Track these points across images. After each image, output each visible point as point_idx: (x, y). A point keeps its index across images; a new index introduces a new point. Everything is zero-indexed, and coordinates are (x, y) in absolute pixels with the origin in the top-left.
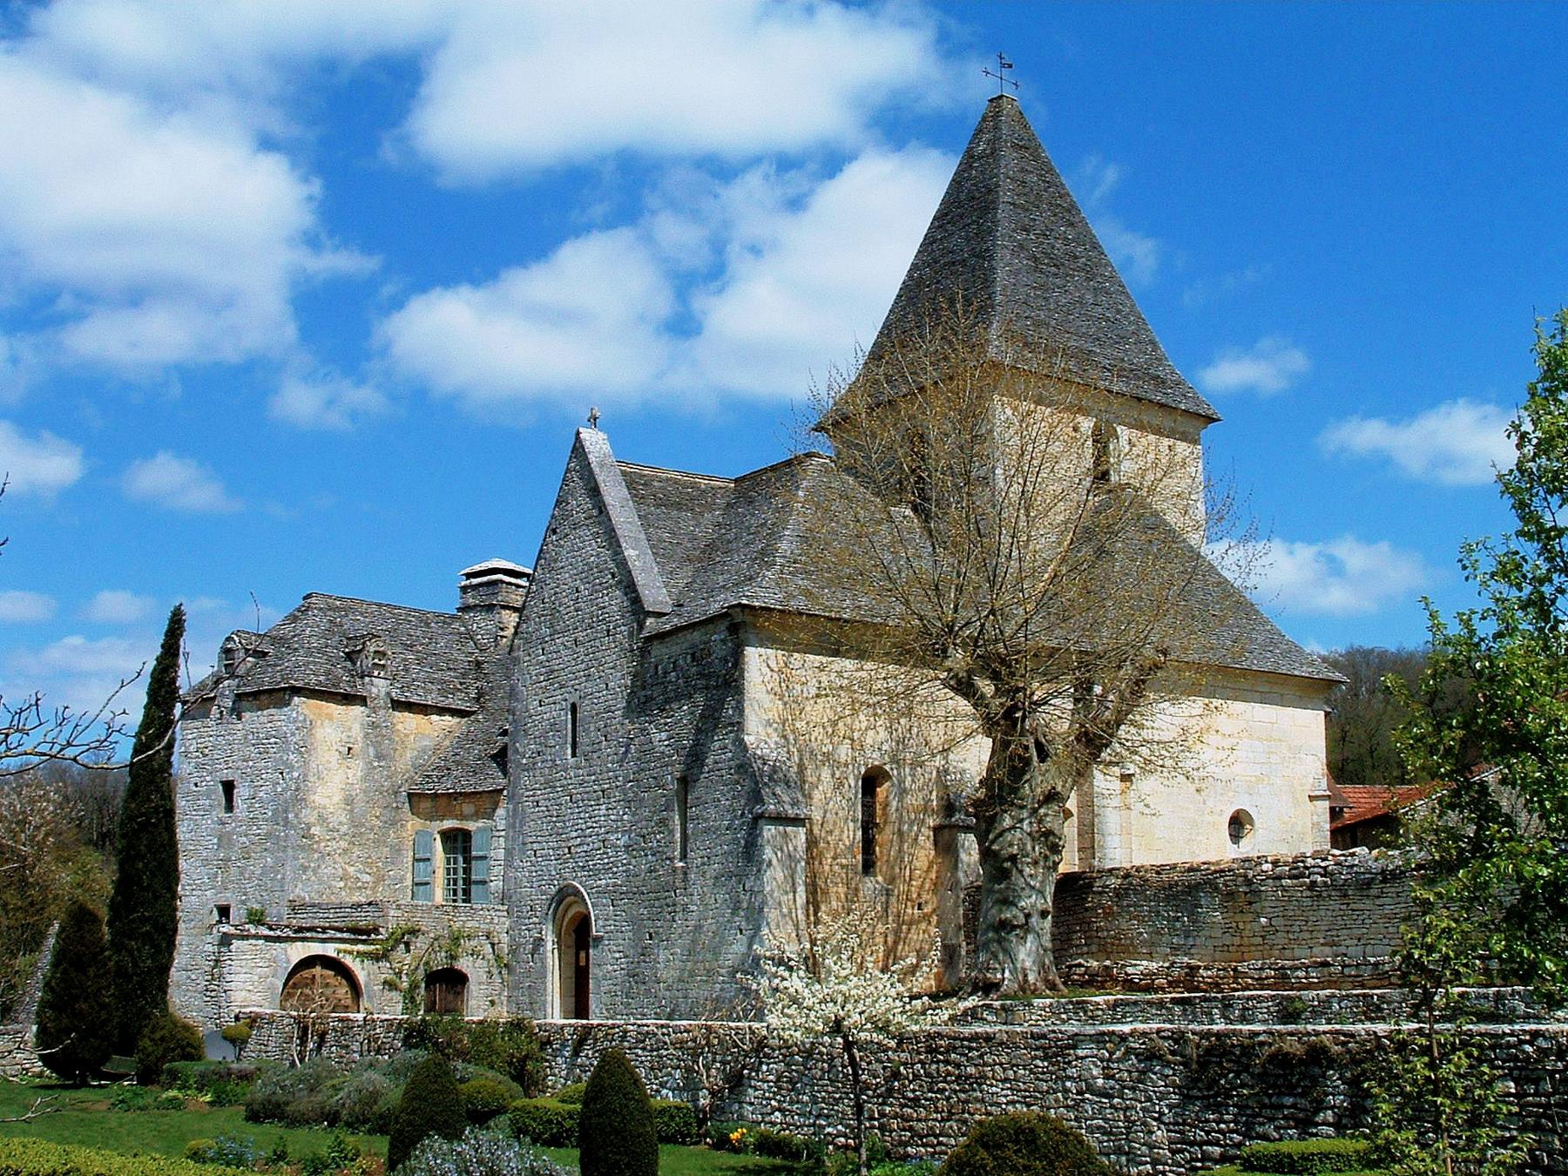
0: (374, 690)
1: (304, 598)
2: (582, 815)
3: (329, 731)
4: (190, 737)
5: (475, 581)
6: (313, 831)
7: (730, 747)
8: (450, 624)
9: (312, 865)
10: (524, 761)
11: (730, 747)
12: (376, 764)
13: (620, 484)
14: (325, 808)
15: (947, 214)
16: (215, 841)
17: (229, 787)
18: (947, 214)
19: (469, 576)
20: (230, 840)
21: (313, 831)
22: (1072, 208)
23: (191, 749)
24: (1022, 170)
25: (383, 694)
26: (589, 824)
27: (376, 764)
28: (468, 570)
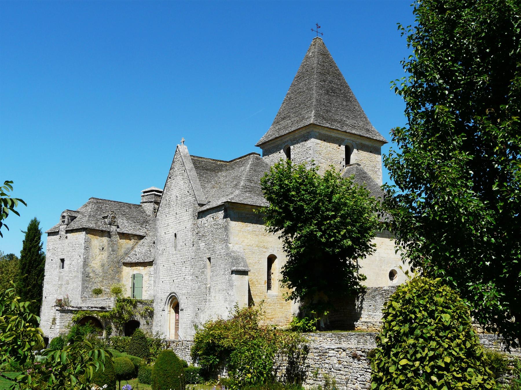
0: (112, 229)
1: (89, 199)
2: (177, 270)
3: (96, 242)
4: (50, 244)
5: (146, 194)
6: (90, 275)
7: (224, 248)
8: (138, 208)
9: (90, 286)
10: (160, 252)
11: (224, 248)
12: (112, 253)
13: (191, 163)
14: (94, 267)
15: (299, 76)
16: (58, 278)
17: (63, 260)
18: (299, 76)
19: (144, 192)
20: (62, 278)
21: (90, 275)
22: (340, 75)
23: (51, 248)
24: (323, 62)
25: (114, 230)
26: (180, 273)
27: (112, 253)
28: (144, 190)
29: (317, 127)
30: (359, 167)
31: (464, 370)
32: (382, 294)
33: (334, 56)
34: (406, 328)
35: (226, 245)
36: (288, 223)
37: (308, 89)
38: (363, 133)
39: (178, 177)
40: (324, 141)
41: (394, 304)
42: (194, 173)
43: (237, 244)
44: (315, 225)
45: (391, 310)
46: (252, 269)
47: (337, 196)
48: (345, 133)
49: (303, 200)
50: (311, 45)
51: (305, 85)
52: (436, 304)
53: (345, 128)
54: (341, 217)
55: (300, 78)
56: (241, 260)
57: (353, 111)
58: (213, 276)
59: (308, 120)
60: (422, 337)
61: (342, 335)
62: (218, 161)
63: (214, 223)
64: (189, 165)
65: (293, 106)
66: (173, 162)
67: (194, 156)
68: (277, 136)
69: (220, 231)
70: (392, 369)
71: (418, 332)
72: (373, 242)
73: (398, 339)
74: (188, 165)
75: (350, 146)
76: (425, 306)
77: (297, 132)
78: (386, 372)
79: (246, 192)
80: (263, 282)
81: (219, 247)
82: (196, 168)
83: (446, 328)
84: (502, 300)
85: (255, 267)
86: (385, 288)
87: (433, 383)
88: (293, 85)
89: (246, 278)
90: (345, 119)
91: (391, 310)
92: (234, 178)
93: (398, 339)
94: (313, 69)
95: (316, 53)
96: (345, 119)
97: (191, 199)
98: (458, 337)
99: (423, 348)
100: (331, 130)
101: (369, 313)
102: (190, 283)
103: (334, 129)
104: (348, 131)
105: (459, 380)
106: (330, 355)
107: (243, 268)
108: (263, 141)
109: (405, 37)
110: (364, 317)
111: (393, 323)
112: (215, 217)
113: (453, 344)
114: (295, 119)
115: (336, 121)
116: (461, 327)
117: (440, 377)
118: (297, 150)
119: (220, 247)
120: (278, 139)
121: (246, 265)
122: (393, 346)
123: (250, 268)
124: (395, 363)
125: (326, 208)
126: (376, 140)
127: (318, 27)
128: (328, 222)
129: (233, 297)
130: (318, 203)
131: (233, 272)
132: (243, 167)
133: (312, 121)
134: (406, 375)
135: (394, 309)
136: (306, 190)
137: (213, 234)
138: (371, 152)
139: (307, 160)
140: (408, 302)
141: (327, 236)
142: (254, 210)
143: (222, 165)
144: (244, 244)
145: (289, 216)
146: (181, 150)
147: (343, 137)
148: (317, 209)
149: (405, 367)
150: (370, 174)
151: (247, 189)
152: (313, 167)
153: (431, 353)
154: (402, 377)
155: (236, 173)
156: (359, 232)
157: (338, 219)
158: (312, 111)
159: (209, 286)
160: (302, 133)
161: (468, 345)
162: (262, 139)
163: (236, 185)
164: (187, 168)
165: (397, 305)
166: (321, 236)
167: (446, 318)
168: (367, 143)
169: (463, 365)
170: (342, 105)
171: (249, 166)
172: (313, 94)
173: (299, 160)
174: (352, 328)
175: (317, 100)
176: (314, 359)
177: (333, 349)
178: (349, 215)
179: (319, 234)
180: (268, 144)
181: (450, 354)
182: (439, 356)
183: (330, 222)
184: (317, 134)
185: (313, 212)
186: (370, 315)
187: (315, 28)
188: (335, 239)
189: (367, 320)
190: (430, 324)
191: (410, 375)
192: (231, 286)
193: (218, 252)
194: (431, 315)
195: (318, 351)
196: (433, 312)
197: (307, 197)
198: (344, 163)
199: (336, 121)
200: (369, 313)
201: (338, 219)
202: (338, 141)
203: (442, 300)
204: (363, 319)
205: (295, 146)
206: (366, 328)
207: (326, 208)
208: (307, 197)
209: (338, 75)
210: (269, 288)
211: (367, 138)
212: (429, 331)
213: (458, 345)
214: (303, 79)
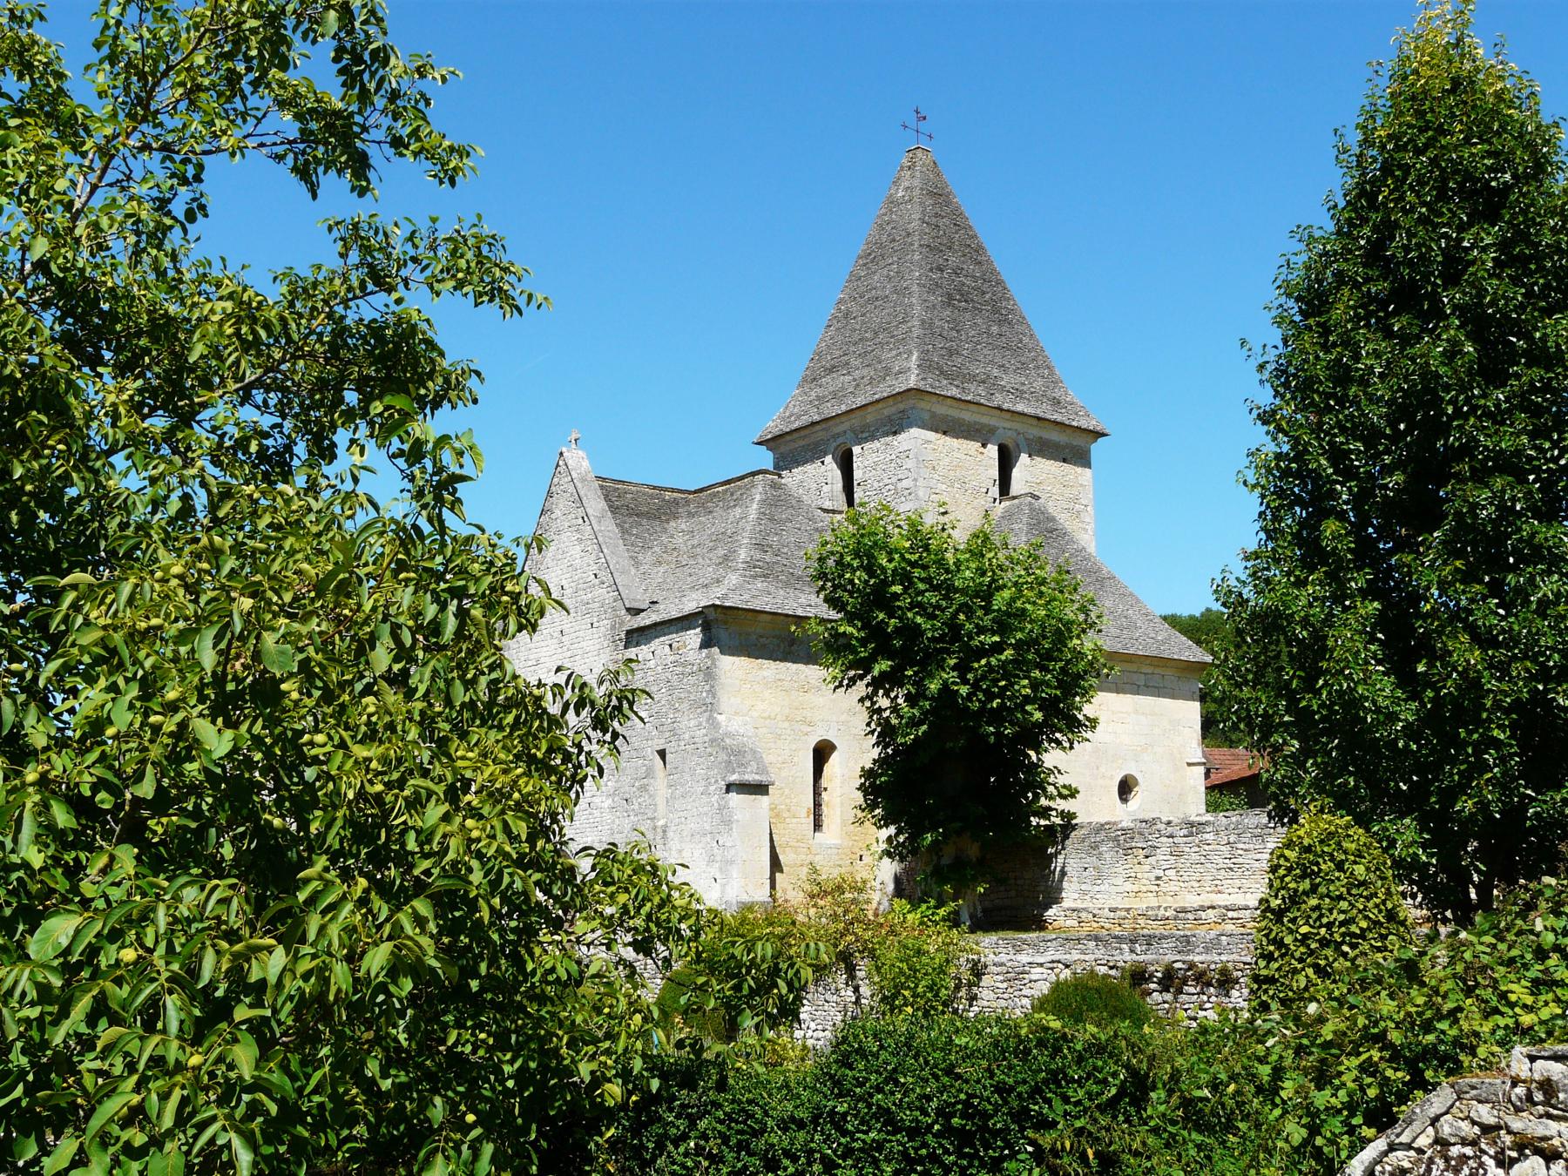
22: (980, 249)
29: (927, 398)
30: (1036, 504)
31: (1383, 937)
32: (1116, 839)
33: (963, 199)
34: (1305, 885)
35: (711, 717)
36: (883, 665)
37: (895, 292)
38: (1045, 411)
39: (564, 537)
40: (945, 433)
41: (1287, 853)
42: (608, 527)
43: (736, 713)
44: (954, 668)
45: (1282, 862)
46: (776, 776)
47: (1006, 594)
48: (998, 412)
49: (921, 608)
50: (902, 169)
51: (890, 279)
52: (1345, 852)
53: (998, 399)
54: (1015, 647)
55: (872, 257)
56: (749, 757)
57: (1017, 350)
58: (673, 797)
59: (902, 377)
60: (1328, 896)
61: (1024, 942)
62: (666, 489)
63: (672, 658)
64: (596, 505)
65: (856, 337)
66: (550, 494)
67: (604, 479)
68: (816, 418)
69: (692, 680)
70: (1288, 940)
71: (1322, 889)
72: (1088, 710)
73: (1295, 899)
74: (593, 503)
75: (1011, 445)
76: (1331, 855)
77: (870, 409)
78: (1279, 943)
79: (755, 577)
80: (803, 813)
81: (691, 724)
82: (614, 509)
83: (1363, 884)
84: (1424, 846)
85: (784, 774)
86: (1124, 824)
87: (1345, 955)
88: (854, 278)
89: (764, 800)
90: (995, 372)
91: (1282, 862)
92: (717, 539)
93: (1295, 899)
94: (909, 234)
95: (917, 192)
96: (995, 372)
97: (604, 594)
98: (1375, 895)
99: (1331, 911)
100: (962, 406)
101: (1084, 887)
102: (608, 817)
103: (969, 402)
104: (1005, 406)
105: (1379, 950)
106: (1034, 977)
107: (757, 777)
108: (776, 432)
109: (1254, 363)
110: (1071, 895)
111: (1287, 879)
112: (675, 645)
113: (1370, 905)
114: (865, 372)
115: (972, 378)
116: (1379, 883)
117: (1353, 946)
118: (873, 458)
119: (692, 723)
120: (818, 427)
121: (763, 770)
122: (1288, 910)
123: (773, 777)
124: (1291, 931)
125: (977, 626)
126: (1078, 428)
127: (919, 119)
128: (983, 662)
129: (733, 851)
130: (955, 615)
131: (729, 788)
132: (738, 510)
133: (913, 381)
134: (1308, 947)
135: (1287, 859)
136: (928, 580)
137: (671, 689)
138: (1064, 461)
139: (900, 485)
140: (1308, 849)
141: (981, 696)
142: (793, 628)
143: (676, 502)
144: (755, 714)
145: (884, 650)
146: (570, 463)
147: (993, 422)
148: (954, 628)
149: (1306, 936)
150: (1064, 520)
151: (761, 570)
152: (942, 519)
153: (1342, 917)
154: (1302, 949)
155: (720, 527)
156: (1061, 684)
157: (1008, 653)
158: (911, 353)
159: (661, 823)
160: (886, 412)
161: (1389, 905)
162: (772, 425)
163: (726, 558)
164: (590, 511)
165: (1292, 855)
166: (969, 696)
167: (1360, 870)
168: (1055, 436)
169: (1383, 931)
170: (989, 335)
171: (755, 506)
172: (911, 305)
173: (876, 485)
174: (1040, 925)
175: (923, 321)
176: (994, 989)
177: (1041, 965)
178: (1036, 642)
179: (964, 690)
180: (788, 438)
181: (1366, 918)
182: (1352, 921)
183: (988, 663)
184: (926, 416)
185: (943, 636)
186: (1085, 893)
187: (911, 120)
188: (1003, 704)
189: (1079, 905)
190: (1338, 879)
191: (1313, 946)
192: (727, 823)
193: (687, 736)
194: (1340, 866)
195: (1004, 969)
196: (1342, 862)
197: (932, 598)
198: (995, 492)
199: (972, 378)
200: (1084, 887)
201: (1008, 653)
202: (981, 435)
203: (1353, 846)
204: (1066, 904)
205: (867, 446)
206: (1075, 923)
207: (977, 626)
208: (932, 598)
209: (975, 252)
210: (818, 826)
211: (1056, 423)
212: (1338, 888)
213: (1377, 906)
214: (882, 263)
